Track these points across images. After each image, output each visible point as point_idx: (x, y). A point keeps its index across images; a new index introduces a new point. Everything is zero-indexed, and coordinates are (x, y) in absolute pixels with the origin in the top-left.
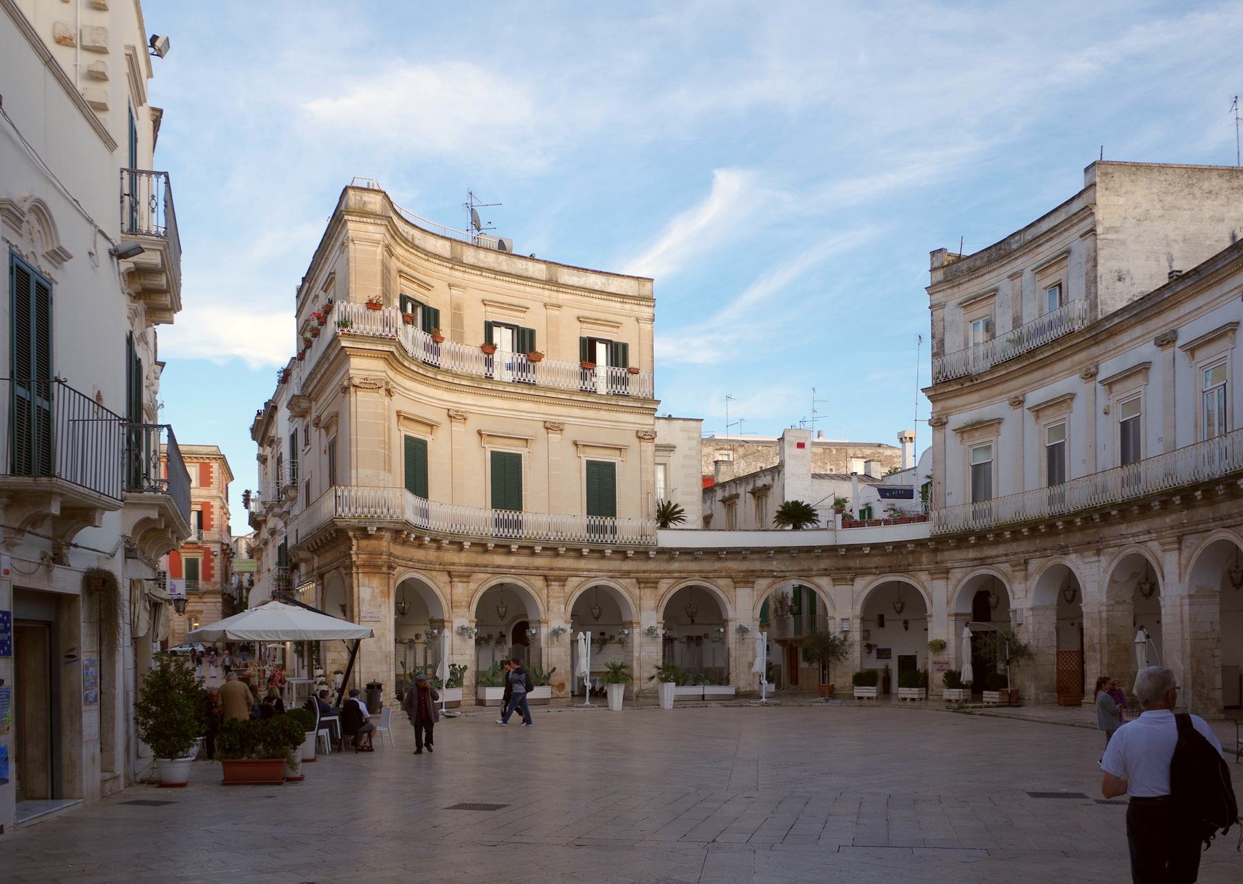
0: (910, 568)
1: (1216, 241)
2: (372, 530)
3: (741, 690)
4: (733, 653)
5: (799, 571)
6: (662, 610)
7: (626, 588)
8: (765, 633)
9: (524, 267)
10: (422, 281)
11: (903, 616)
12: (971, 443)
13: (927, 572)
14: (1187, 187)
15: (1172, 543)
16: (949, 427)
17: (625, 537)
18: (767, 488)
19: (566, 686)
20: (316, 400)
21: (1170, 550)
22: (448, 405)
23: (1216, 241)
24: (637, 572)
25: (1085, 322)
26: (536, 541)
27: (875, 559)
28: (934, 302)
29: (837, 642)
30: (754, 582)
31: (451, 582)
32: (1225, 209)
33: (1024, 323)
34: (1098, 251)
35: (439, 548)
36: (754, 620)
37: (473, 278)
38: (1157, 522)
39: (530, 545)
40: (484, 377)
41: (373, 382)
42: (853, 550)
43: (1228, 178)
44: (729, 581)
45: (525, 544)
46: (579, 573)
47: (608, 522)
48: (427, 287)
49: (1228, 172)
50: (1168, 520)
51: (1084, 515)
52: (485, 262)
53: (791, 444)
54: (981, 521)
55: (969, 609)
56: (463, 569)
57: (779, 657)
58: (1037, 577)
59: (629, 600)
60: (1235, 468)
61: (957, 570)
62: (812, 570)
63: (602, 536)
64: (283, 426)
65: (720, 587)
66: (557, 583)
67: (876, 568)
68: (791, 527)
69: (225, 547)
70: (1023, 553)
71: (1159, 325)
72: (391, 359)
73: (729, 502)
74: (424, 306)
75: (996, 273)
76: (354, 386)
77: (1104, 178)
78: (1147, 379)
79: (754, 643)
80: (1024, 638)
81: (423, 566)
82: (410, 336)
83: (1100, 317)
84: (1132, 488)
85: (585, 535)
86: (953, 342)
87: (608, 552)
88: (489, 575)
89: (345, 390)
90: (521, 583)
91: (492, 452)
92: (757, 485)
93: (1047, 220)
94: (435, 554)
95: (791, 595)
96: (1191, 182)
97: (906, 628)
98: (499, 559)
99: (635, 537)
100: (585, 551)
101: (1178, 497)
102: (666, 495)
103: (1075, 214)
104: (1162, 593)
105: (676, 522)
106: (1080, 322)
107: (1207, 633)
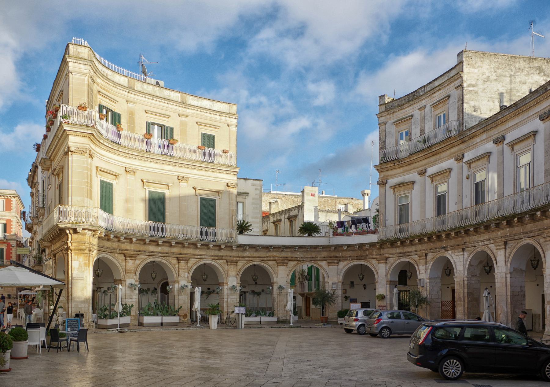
0: (367, 257)
1: (522, 94)
2: (79, 230)
3: (280, 319)
4: (276, 300)
5: (310, 258)
6: (239, 277)
7: (220, 265)
8: (293, 290)
9: (168, 94)
10: (112, 98)
11: (364, 282)
12: (399, 194)
13: (376, 260)
14: (508, 65)
15: (502, 245)
16: (387, 186)
17: (220, 238)
18: (296, 216)
19: (188, 316)
20: (53, 160)
21: (500, 249)
22: (126, 165)
23: (522, 94)
24: (226, 256)
25: (457, 132)
26: (172, 239)
27: (349, 252)
28: (380, 122)
29: (330, 295)
30: (287, 263)
31: (125, 260)
32: (526, 78)
33: (426, 133)
34: (464, 96)
35: (119, 241)
36: (287, 283)
37: (140, 98)
38: (494, 234)
39: (169, 241)
40: (145, 151)
41: (82, 150)
42: (338, 247)
43: (528, 62)
44: (274, 262)
45: (166, 240)
46: (196, 256)
47: (211, 230)
48: (115, 101)
49: (528, 59)
50: (499, 233)
51: (456, 231)
52: (147, 91)
53: (308, 194)
54: (403, 233)
55: (397, 279)
56: (132, 253)
57: (300, 302)
58: (432, 263)
59: (222, 271)
60: (538, 205)
61: (391, 259)
62: (317, 257)
63: (208, 237)
64: (40, 176)
65: (269, 266)
66: (184, 262)
67: (350, 257)
68: (307, 235)
69: (19, 243)
70: (425, 250)
71: (495, 133)
72: (92, 137)
73: (276, 223)
74: (112, 112)
75: (412, 107)
76: (72, 152)
77: (467, 59)
78: (489, 161)
79: (287, 295)
80: (424, 294)
81: (110, 251)
82: (104, 127)
83: (465, 129)
84: (481, 217)
85: (199, 236)
86: (390, 142)
87: (211, 246)
88: (147, 257)
89: (66, 153)
90: (164, 261)
91: (149, 191)
92: (290, 215)
93: (438, 80)
94: (117, 244)
95: (307, 271)
96: (510, 63)
97: (365, 289)
98: (152, 248)
99: (225, 238)
100: (199, 245)
101: (505, 221)
102: (243, 217)
103: (452, 77)
104: (496, 271)
105: (247, 231)
106: (455, 132)
107: (519, 292)
